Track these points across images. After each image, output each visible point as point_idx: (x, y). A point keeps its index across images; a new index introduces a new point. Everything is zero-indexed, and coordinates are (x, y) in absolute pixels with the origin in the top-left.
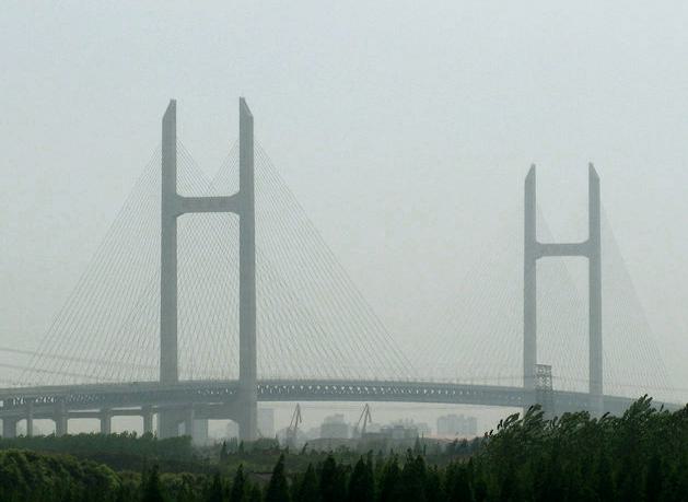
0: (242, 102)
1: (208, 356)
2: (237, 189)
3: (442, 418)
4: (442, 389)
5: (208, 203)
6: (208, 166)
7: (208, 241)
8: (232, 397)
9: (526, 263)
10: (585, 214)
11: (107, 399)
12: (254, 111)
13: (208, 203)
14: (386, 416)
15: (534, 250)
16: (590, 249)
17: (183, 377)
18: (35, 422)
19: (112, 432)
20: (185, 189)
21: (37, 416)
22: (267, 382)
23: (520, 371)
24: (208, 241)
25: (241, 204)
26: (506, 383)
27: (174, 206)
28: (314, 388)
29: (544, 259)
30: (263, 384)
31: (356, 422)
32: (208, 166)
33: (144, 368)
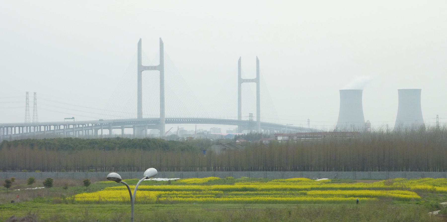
0: (257, 57)
1: (151, 111)
2: (159, 64)
3: (212, 128)
4: (79, 125)
5: (150, 68)
6: (249, 72)
7: (151, 78)
8: (156, 123)
9: (138, 74)
10: (255, 69)
11: (122, 124)
12: (259, 59)
13: (150, 68)
14: (206, 128)
15: (241, 81)
16: (257, 80)
17: (144, 117)
18: (104, 130)
19: (366, 121)
20: (144, 64)
21: (104, 128)
22: (167, 118)
23: (237, 115)
24: (151, 78)
25: (160, 68)
26: (233, 119)
27: (141, 69)
28: (173, 120)
29: (244, 83)
30: (166, 119)
31: (191, 130)
32: (249, 72)
33: (134, 116)
